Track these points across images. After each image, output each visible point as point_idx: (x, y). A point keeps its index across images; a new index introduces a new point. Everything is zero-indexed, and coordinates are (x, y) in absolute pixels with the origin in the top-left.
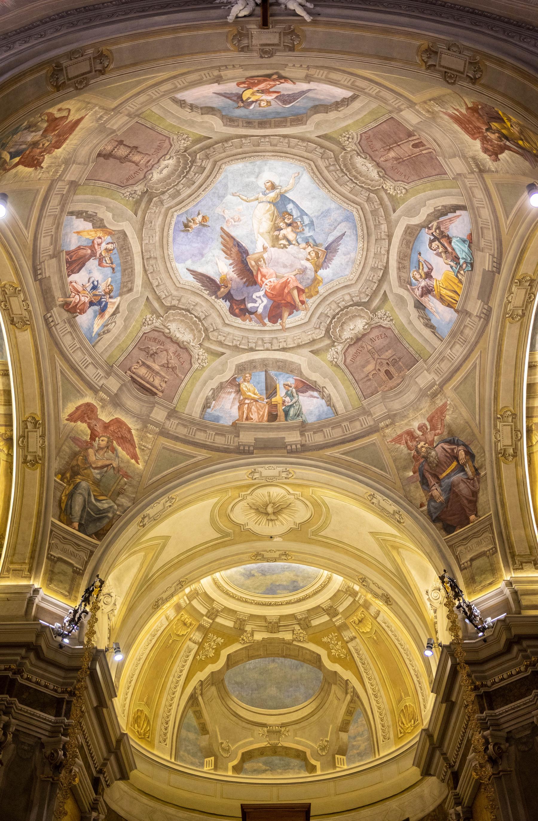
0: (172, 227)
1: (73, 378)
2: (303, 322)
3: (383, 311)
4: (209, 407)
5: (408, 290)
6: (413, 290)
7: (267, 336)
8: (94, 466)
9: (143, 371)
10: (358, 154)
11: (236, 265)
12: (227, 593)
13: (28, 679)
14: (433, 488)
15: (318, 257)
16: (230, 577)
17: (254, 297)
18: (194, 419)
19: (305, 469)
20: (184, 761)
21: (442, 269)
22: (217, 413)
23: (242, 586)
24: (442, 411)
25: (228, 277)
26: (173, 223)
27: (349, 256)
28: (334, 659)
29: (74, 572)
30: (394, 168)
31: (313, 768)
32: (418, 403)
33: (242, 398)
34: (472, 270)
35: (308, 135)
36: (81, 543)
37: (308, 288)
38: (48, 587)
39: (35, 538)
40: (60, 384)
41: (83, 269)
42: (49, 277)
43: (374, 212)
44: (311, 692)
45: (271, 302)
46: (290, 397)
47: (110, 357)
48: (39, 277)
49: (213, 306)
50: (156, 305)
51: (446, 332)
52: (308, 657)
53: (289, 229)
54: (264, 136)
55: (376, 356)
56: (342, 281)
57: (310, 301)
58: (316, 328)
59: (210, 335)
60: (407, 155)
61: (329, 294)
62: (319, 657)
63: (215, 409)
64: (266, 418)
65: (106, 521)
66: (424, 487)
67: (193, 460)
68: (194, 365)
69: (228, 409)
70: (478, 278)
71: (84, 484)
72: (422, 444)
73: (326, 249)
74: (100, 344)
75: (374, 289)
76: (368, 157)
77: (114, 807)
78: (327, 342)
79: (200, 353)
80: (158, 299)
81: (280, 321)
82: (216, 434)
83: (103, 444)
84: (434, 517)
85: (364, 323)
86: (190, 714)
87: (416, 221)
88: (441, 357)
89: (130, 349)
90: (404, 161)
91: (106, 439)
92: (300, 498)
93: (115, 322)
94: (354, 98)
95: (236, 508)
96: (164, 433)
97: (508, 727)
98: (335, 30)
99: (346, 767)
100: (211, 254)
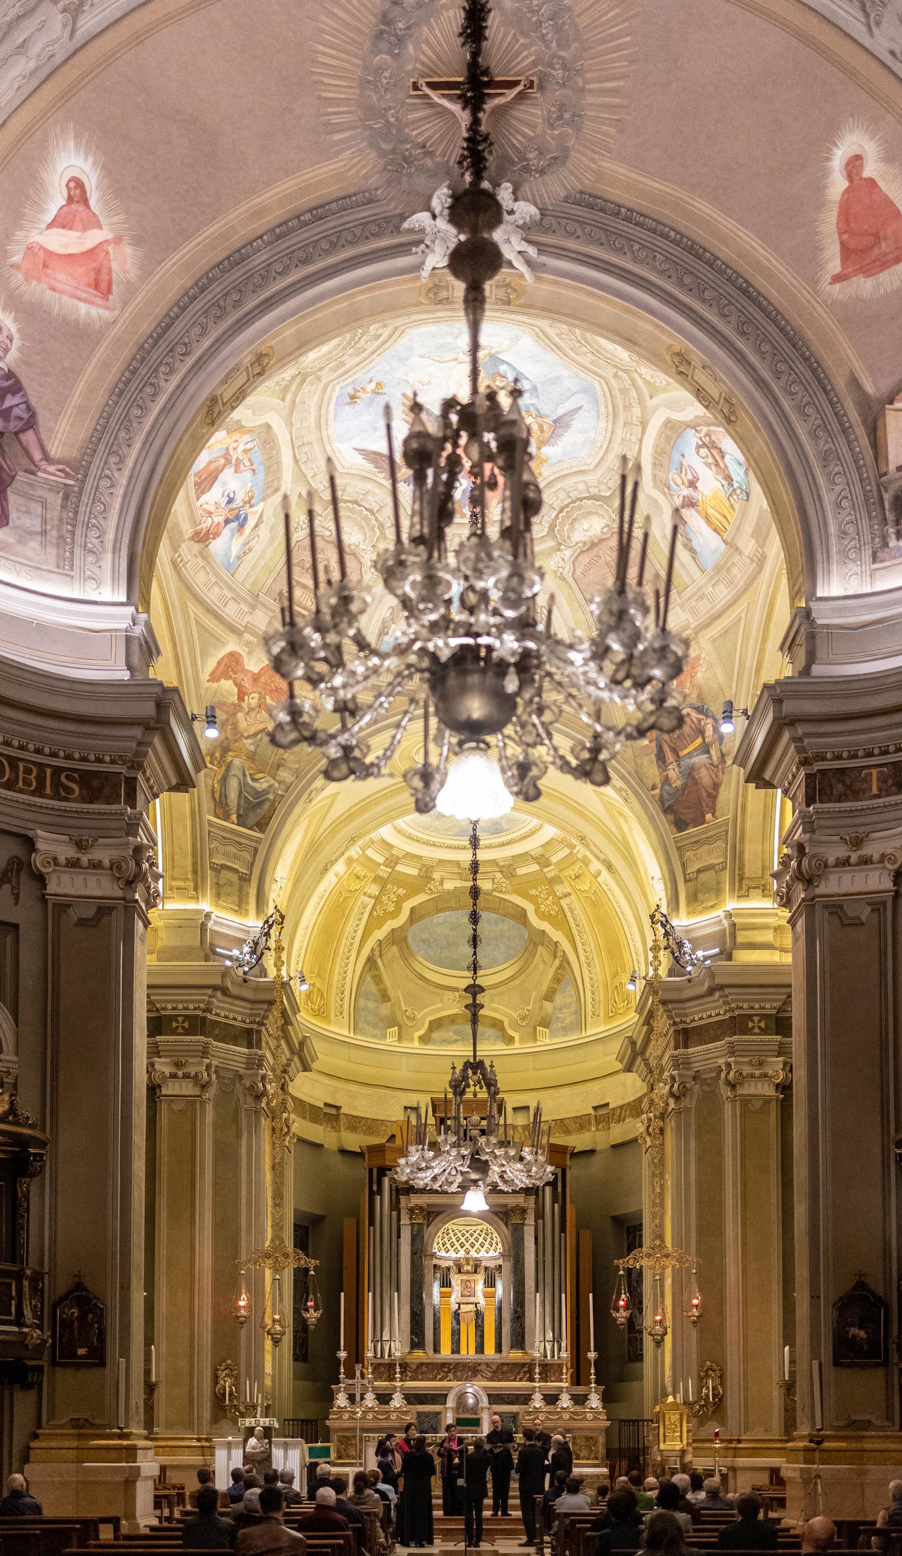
0: (333, 402)
1: (211, 624)
4: (387, 634)
5: (665, 494)
6: (671, 495)
8: (246, 735)
12: (410, 837)
13: (217, 1014)
15: (542, 431)
20: (365, 1034)
26: (335, 396)
28: (542, 916)
29: (241, 879)
31: (510, 1040)
36: (242, 841)
38: (217, 905)
39: (194, 846)
40: (196, 637)
44: (513, 952)
51: (709, 563)
52: (511, 910)
61: (556, 479)
62: (524, 911)
65: (267, 806)
71: (237, 762)
73: (554, 422)
77: (297, 1094)
78: (550, 543)
83: (254, 702)
84: (666, 806)
86: (368, 979)
88: (700, 593)
91: (256, 695)
97: (697, 1067)
98: (564, 292)
99: (548, 1041)
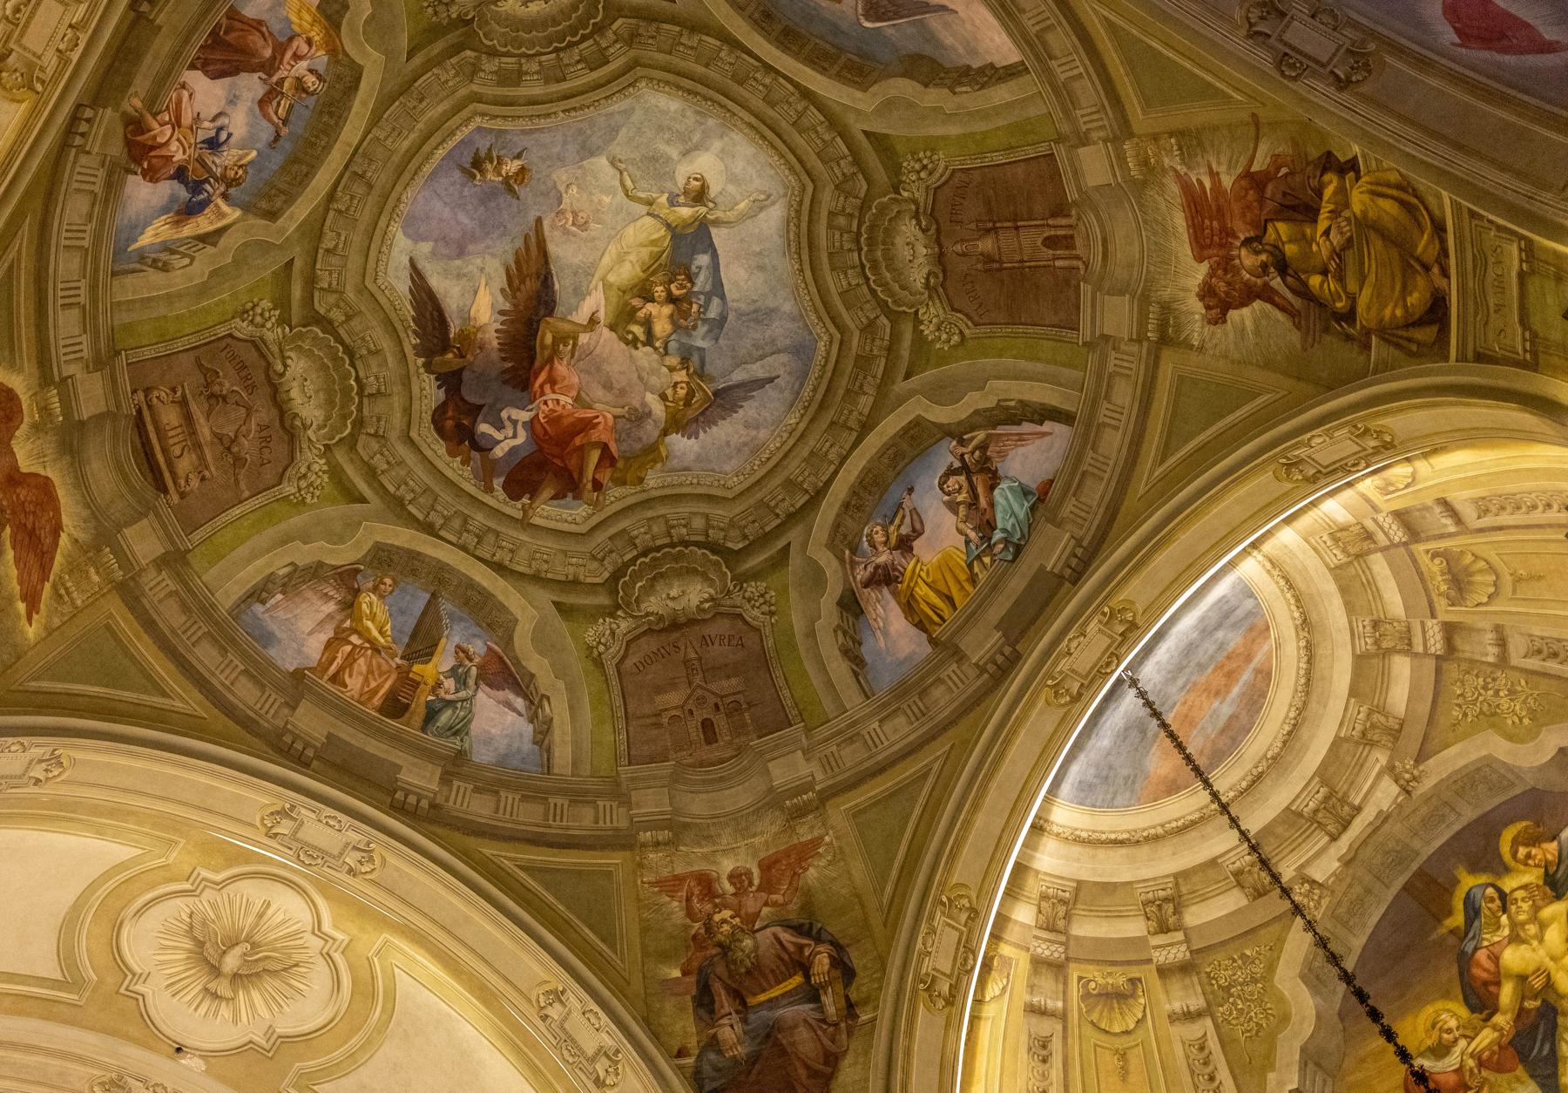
0: (450, 144)
2: (573, 528)
3: (762, 585)
4: (263, 602)
5: (842, 560)
6: (853, 564)
7: (480, 518)
9: (170, 417)
10: (916, 216)
11: (512, 322)
14: (725, 1021)
17: (504, 414)
18: (213, 605)
19: (414, 863)
21: (943, 536)
22: (273, 627)
24: (805, 852)
25: (479, 335)
26: (459, 137)
27: (754, 433)
30: (969, 279)
32: (751, 818)
34: (1013, 561)
35: (850, 119)
37: (627, 459)
41: (227, 81)
42: (160, 28)
43: (864, 362)
45: (535, 448)
46: (458, 681)
47: (128, 327)
49: (406, 382)
50: (297, 292)
51: (885, 681)
53: (667, 310)
54: (769, 68)
55: (698, 680)
56: (708, 481)
57: (615, 492)
58: (594, 558)
59: (362, 439)
60: (1018, 258)
63: (276, 614)
64: (377, 701)
66: (702, 1012)
67: (158, 701)
68: (285, 483)
69: (303, 630)
70: (1017, 583)
72: (727, 914)
73: (716, 394)
74: (129, 280)
75: (768, 529)
76: (933, 231)
78: (603, 600)
79: (316, 467)
80: (311, 281)
81: (525, 500)
82: (246, 672)
85: (706, 596)
87: (941, 415)
88: (850, 733)
89: (179, 345)
90: (1000, 270)
92: (337, 957)
93: (193, 259)
94: (1011, 72)
95: (156, 912)
100: (479, 261)
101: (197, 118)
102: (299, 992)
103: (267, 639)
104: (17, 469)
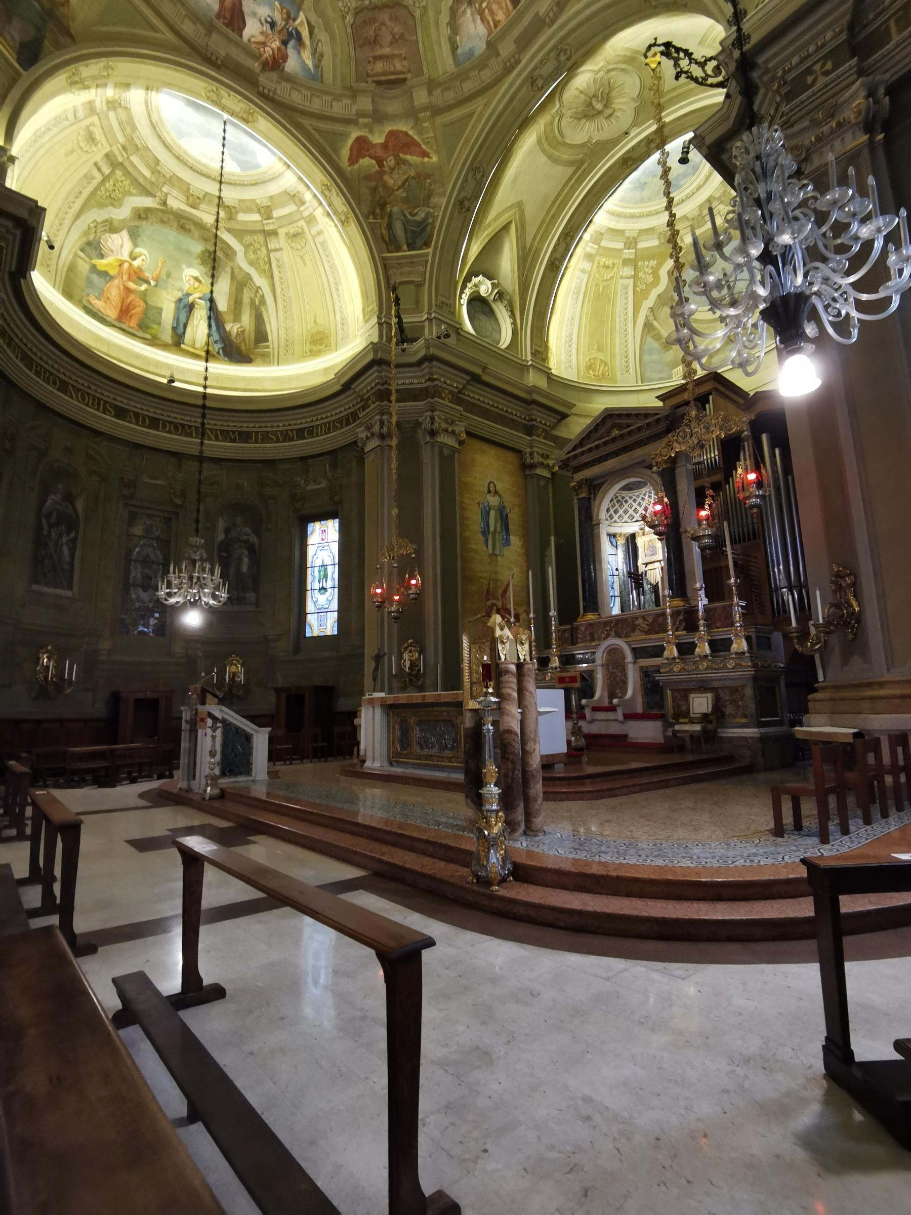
1: (322, 125)
8: (395, 188)
9: (379, 66)
16: (622, 200)
18: (452, 74)
22: (468, 47)
23: (642, 201)
33: (477, 5)
48: (219, 62)
71: (395, 209)
74: (325, 75)
86: (649, 340)
89: (353, 55)
91: (392, 158)
96: (437, 111)
101: (262, 33)
102: (621, 85)
103: (471, 52)
104: (381, 144)
